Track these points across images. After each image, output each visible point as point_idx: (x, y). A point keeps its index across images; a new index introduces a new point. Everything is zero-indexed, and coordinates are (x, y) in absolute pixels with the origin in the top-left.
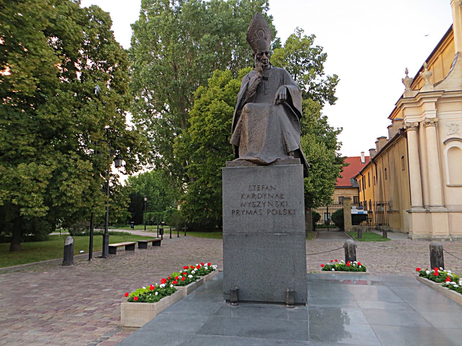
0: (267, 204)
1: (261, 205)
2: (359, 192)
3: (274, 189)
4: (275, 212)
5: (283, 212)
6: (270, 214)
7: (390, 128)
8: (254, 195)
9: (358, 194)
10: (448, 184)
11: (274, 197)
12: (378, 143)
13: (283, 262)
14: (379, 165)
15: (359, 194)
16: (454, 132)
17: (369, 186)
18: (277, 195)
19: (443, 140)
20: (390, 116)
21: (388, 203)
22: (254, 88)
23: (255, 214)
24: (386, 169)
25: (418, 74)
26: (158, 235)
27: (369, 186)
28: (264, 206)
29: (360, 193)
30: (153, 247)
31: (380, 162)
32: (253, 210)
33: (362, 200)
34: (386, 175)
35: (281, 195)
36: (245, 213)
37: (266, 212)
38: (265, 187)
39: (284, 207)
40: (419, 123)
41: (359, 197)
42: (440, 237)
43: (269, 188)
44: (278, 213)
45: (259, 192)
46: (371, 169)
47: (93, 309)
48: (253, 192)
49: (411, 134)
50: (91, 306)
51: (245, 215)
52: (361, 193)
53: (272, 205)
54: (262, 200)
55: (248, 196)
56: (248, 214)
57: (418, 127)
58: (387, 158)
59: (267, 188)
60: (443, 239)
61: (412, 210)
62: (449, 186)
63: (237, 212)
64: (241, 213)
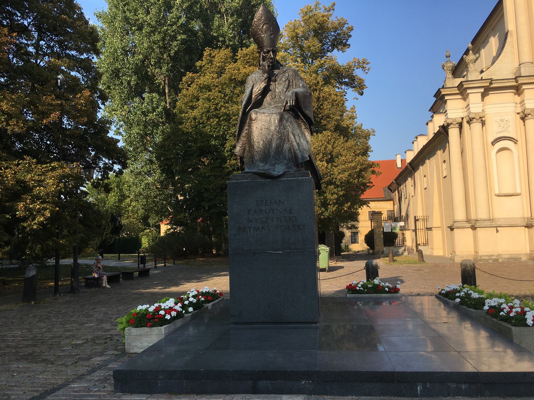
10: (497, 192)
16: (504, 129)
19: (491, 139)
20: (432, 108)
22: (260, 92)
23: (263, 230)
25: (462, 59)
26: (139, 264)
30: (467, 100)
36: (252, 229)
38: (273, 201)
40: (462, 118)
42: (487, 258)
47: (79, 342)
49: (453, 132)
50: (77, 339)
55: (255, 212)
57: (461, 126)
59: (275, 202)
60: (491, 259)
61: (455, 225)
62: (498, 196)
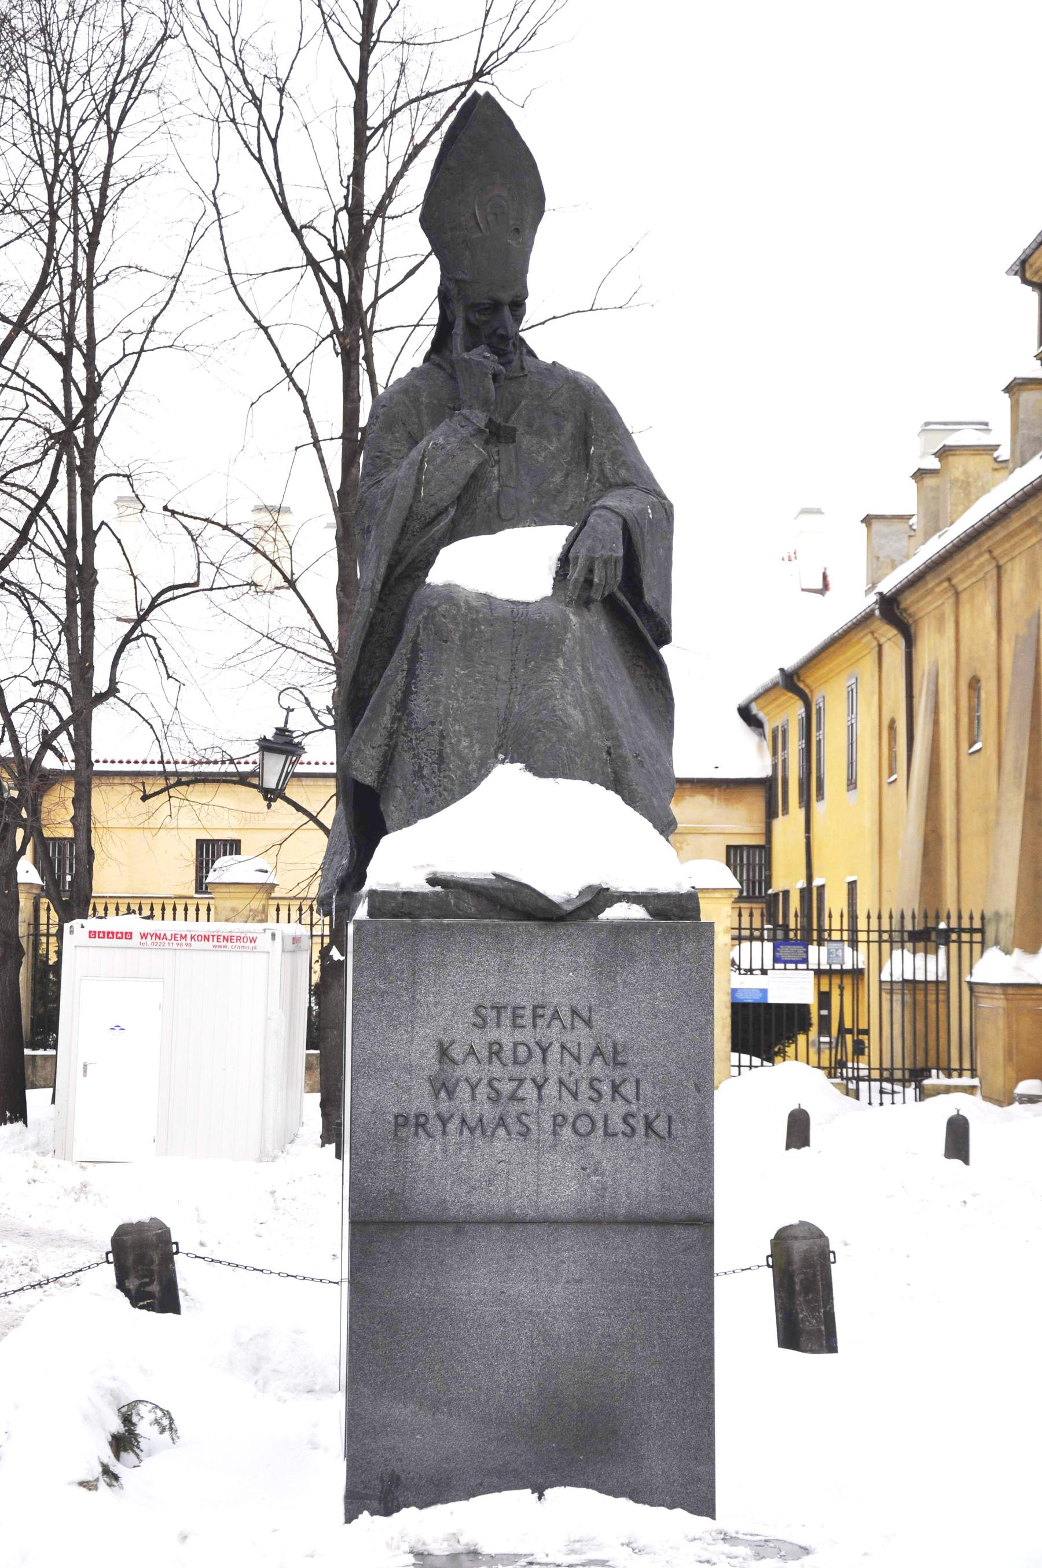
0: (551, 1089)
1: (528, 1091)
2: (771, 814)
3: (588, 1023)
4: (583, 1125)
5: (621, 1127)
6: (567, 1132)
7: (1027, 397)
8: (495, 1051)
9: (761, 828)
11: (585, 1059)
12: (930, 481)
13: (615, 1345)
14: (934, 647)
15: (768, 833)
17: (852, 784)
18: (598, 1052)
21: (977, 924)
24: (975, 684)
27: (852, 784)
28: (540, 1098)
29: (779, 824)
31: (941, 620)
32: (490, 1112)
33: (787, 876)
34: (974, 720)
35: (616, 1052)
36: (453, 1126)
37: (548, 1125)
38: (549, 1012)
39: (629, 1102)
41: (766, 849)
43: (565, 1013)
44: (601, 1132)
45: (519, 1036)
46: (869, 663)
48: (493, 1034)
51: (453, 1138)
52: (788, 830)
53: (575, 1096)
54: (534, 1068)
56: (466, 1132)
58: (989, 610)
59: (556, 1016)
63: (418, 1125)
64: (435, 1126)
